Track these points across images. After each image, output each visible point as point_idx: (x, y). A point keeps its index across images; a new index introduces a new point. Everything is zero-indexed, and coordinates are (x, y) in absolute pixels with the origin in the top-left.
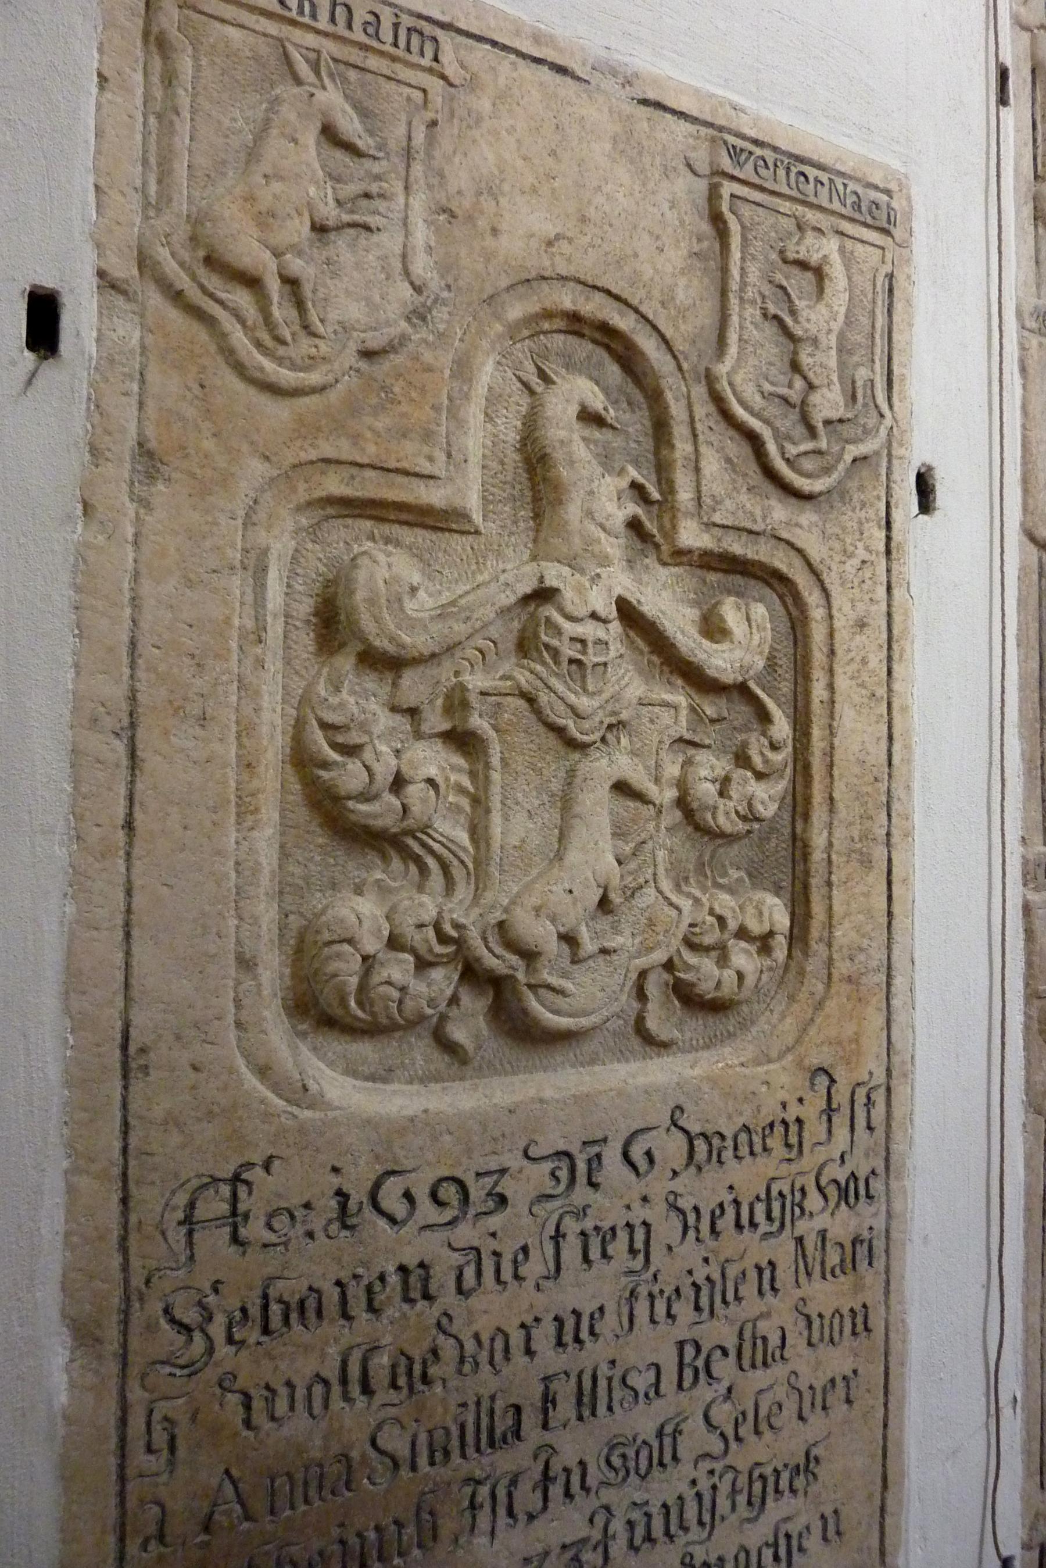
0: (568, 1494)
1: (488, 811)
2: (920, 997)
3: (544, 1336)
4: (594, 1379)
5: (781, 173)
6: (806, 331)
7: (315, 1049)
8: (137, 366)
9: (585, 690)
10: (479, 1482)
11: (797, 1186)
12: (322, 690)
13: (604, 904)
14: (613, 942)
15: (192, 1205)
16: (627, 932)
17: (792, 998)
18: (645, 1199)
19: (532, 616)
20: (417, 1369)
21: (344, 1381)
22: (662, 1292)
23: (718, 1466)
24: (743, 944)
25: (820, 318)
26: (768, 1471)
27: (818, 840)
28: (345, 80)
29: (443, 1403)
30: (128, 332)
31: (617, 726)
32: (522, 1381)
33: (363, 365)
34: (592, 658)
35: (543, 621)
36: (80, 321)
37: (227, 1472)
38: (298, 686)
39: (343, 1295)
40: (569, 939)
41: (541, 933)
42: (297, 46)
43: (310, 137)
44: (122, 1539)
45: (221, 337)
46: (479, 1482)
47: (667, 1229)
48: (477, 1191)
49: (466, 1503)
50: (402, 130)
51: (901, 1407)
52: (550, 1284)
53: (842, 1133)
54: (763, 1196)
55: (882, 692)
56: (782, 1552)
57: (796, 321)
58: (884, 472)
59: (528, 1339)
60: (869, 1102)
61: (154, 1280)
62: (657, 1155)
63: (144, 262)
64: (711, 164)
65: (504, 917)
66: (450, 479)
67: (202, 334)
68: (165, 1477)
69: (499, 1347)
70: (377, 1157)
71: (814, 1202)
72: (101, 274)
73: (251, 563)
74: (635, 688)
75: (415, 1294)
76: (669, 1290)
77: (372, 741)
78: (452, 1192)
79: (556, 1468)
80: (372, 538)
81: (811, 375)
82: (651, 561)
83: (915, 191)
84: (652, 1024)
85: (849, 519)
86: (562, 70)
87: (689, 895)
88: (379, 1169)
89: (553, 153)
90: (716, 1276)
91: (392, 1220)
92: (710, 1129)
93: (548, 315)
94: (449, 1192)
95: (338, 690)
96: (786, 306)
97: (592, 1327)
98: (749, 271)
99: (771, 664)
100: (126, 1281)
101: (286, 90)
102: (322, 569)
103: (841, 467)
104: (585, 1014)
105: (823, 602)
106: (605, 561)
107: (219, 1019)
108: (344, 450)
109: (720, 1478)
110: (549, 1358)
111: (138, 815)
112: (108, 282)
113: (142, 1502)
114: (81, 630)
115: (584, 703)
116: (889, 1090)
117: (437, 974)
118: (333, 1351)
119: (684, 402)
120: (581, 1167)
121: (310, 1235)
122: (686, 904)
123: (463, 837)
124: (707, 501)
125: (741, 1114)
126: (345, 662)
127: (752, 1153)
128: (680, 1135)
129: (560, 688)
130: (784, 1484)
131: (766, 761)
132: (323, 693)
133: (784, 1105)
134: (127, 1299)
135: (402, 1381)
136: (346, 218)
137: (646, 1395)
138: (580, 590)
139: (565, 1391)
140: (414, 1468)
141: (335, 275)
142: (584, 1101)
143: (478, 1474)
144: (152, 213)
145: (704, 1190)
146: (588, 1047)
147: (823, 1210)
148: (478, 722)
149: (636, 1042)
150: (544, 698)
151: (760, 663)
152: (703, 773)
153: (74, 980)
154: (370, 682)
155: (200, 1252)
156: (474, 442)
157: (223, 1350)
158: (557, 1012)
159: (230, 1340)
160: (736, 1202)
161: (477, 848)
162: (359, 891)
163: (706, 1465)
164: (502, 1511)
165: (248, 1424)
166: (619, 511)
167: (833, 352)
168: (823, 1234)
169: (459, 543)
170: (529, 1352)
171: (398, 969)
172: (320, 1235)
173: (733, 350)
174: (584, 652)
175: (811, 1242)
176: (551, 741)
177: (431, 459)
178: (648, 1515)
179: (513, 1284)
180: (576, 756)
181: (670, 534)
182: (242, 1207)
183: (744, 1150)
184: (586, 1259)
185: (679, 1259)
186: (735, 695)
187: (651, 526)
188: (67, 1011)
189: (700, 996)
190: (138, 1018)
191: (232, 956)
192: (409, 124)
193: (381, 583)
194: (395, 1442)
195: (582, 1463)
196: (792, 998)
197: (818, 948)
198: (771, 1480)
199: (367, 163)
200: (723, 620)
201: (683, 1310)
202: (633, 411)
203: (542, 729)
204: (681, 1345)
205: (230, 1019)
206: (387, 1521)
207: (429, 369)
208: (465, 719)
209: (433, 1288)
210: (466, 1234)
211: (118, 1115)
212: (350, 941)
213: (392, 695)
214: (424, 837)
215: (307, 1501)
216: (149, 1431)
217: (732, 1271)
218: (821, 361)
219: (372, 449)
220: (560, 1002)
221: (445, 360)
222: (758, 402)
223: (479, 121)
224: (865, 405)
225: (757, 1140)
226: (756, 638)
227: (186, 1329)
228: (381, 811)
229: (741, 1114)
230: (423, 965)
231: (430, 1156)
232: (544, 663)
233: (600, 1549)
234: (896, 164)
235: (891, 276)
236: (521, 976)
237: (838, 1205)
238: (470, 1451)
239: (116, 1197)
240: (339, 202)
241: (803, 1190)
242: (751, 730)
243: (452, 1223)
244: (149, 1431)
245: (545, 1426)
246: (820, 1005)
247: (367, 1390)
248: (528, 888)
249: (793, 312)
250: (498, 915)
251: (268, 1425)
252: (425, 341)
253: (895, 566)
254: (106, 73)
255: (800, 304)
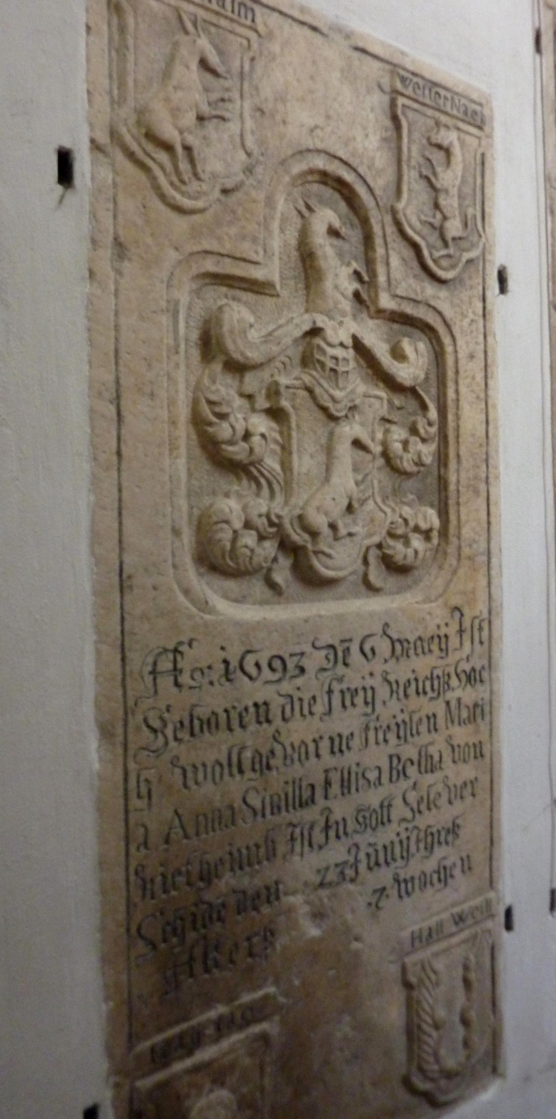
0: (338, 837)
1: (290, 453)
2: (505, 570)
3: (325, 745)
4: (349, 773)
5: (427, 92)
6: (442, 185)
7: (208, 583)
8: (112, 194)
9: (337, 386)
10: (294, 826)
11: (446, 672)
12: (206, 381)
13: (350, 509)
14: (354, 529)
15: (155, 664)
16: (360, 525)
17: (440, 567)
18: (371, 674)
19: (309, 344)
20: (264, 760)
21: (230, 765)
22: (381, 727)
23: (410, 826)
24: (417, 535)
25: (448, 178)
26: (434, 830)
27: (452, 478)
28: (210, 33)
29: (277, 780)
30: (106, 174)
31: (353, 408)
32: (313, 770)
33: (223, 198)
34: (341, 369)
35: (315, 347)
36: (83, 166)
37: (176, 812)
38: (193, 379)
39: (228, 717)
40: (333, 527)
41: (319, 521)
42: (185, 12)
43: (194, 65)
44: (127, 845)
45: (154, 179)
46: (294, 826)
47: (383, 692)
48: (291, 664)
49: (289, 837)
50: (237, 63)
51: (499, 800)
52: (326, 718)
53: (467, 644)
54: (429, 676)
55: (482, 395)
56: (442, 877)
57: (437, 179)
58: (481, 268)
59: (317, 748)
60: (481, 629)
61: (139, 703)
62: (377, 651)
63: (114, 134)
64: (391, 86)
65: (301, 512)
66: (266, 265)
67: (141, 176)
68: (146, 812)
69: (303, 752)
70: (242, 642)
71: (454, 682)
72: (93, 141)
73: (171, 307)
74: (362, 388)
75: (262, 719)
76: (384, 726)
77: (233, 412)
78: (278, 663)
79: (332, 821)
80: (226, 296)
81: (445, 211)
82: (364, 315)
83: (495, 104)
84: (372, 578)
85: (465, 295)
86: (314, 29)
87: (389, 506)
88: (243, 649)
89: (312, 78)
90: (407, 720)
91: (250, 678)
92: (402, 637)
93: (311, 171)
94: (277, 664)
95: (214, 382)
96: (431, 171)
97: (348, 743)
98: (413, 150)
99: (427, 379)
100: (125, 702)
101: (180, 37)
102: (203, 313)
103: (461, 265)
104: (341, 569)
105: (452, 343)
106: (344, 314)
107: (165, 561)
108: (215, 246)
109: (411, 832)
110: (328, 760)
111: (123, 448)
112: (95, 146)
113: (137, 824)
114: (91, 342)
115: (338, 394)
116: (490, 622)
117: (267, 544)
118: (224, 748)
119: (380, 225)
120: (340, 654)
121: (211, 683)
122: (388, 510)
123: (277, 467)
124: (393, 282)
125: (417, 630)
126: (217, 367)
127: (423, 653)
128: (388, 641)
129: (325, 385)
130: (442, 839)
131: (427, 432)
132: (207, 384)
133: (439, 627)
134: (126, 713)
135: (257, 767)
136: (214, 113)
137: (375, 784)
138: (335, 330)
139: (335, 777)
140: (264, 816)
141: (208, 145)
142: (340, 617)
143: (295, 821)
144: (116, 106)
145: (401, 672)
146: (341, 589)
147: (459, 687)
148: (285, 403)
149: (363, 588)
150: (318, 390)
151: (422, 376)
152: (396, 437)
153: (95, 537)
154: (229, 379)
155: (160, 688)
156: (276, 244)
157: (172, 744)
158: (327, 567)
159: (176, 739)
160: (416, 680)
161: (285, 474)
162: (227, 495)
163: (404, 825)
164: (306, 843)
165: (185, 786)
166: (350, 286)
167: (456, 198)
168: (459, 700)
169: (269, 302)
170: (318, 756)
171: (249, 539)
172: (216, 684)
173: (405, 195)
174: (337, 365)
175: (453, 704)
176: (320, 415)
177: (257, 252)
178: (376, 851)
179: (309, 717)
180: (332, 424)
181: (375, 300)
182: (179, 666)
183: (419, 650)
184: (344, 706)
185: (390, 709)
186: (409, 395)
187: (364, 296)
188: (93, 554)
189: (395, 563)
190: (128, 559)
191: (170, 527)
192: (242, 59)
193: (235, 322)
194: (255, 801)
195: (344, 820)
196: (440, 567)
197: (453, 540)
198: (436, 836)
199: (222, 81)
200: (403, 350)
201: (392, 737)
202: (353, 230)
203: (316, 409)
204: (391, 757)
205: (170, 562)
206: (251, 844)
207: (254, 201)
208: (278, 401)
209: (271, 717)
210: (286, 687)
211: (119, 612)
212: (227, 522)
213: (240, 387)
214: (260, 467)
215: (214, 830)
216: (138, 787)
217: (415, 718)
218: (450, 203)
219: (228, 246)
220: (329, 562)
221: (261, 196)
222: (418, 225)
223: (274, 58)
224: (472, 230)
225: (426, 645)
226: (421, 360)
227: (154, 731)
228: (238, 451)
229: (417, 630)
230: (261, 538)
231: (267, 643)
232: (315, 369)
233: (354, 868)
234: (484, 87)
235: (483, 155)
236: (310, 546)
237: (466, 685)
238: (291, 808)
239: (119, 657)
240: (209, 104)
241: (449, 675)
242: (417, 414)
243: (279, 681)
244: (138, 787)
245: (326, 797)
246: (454, 572)
247: (241, 771)
248: (312, 497)
249: (435, 174)
250: (297, 512)
251: (194, 787)
252: (252, 185)
253: (488, 325)
254: (92, 25)
255: (439, 169)
